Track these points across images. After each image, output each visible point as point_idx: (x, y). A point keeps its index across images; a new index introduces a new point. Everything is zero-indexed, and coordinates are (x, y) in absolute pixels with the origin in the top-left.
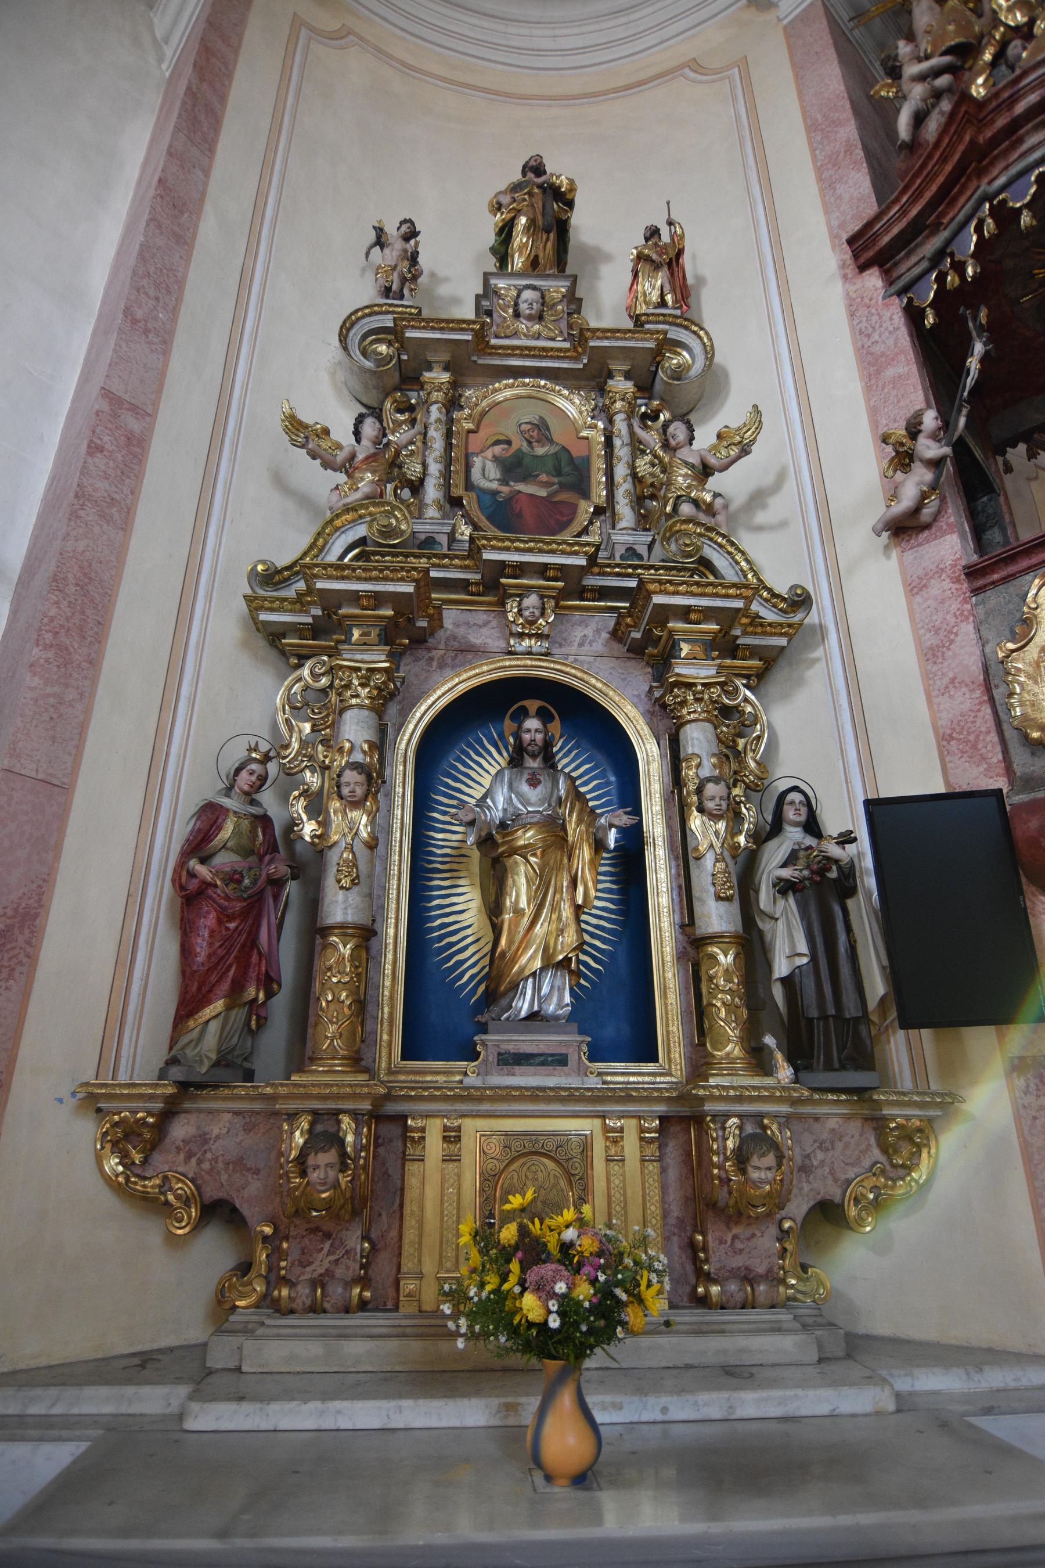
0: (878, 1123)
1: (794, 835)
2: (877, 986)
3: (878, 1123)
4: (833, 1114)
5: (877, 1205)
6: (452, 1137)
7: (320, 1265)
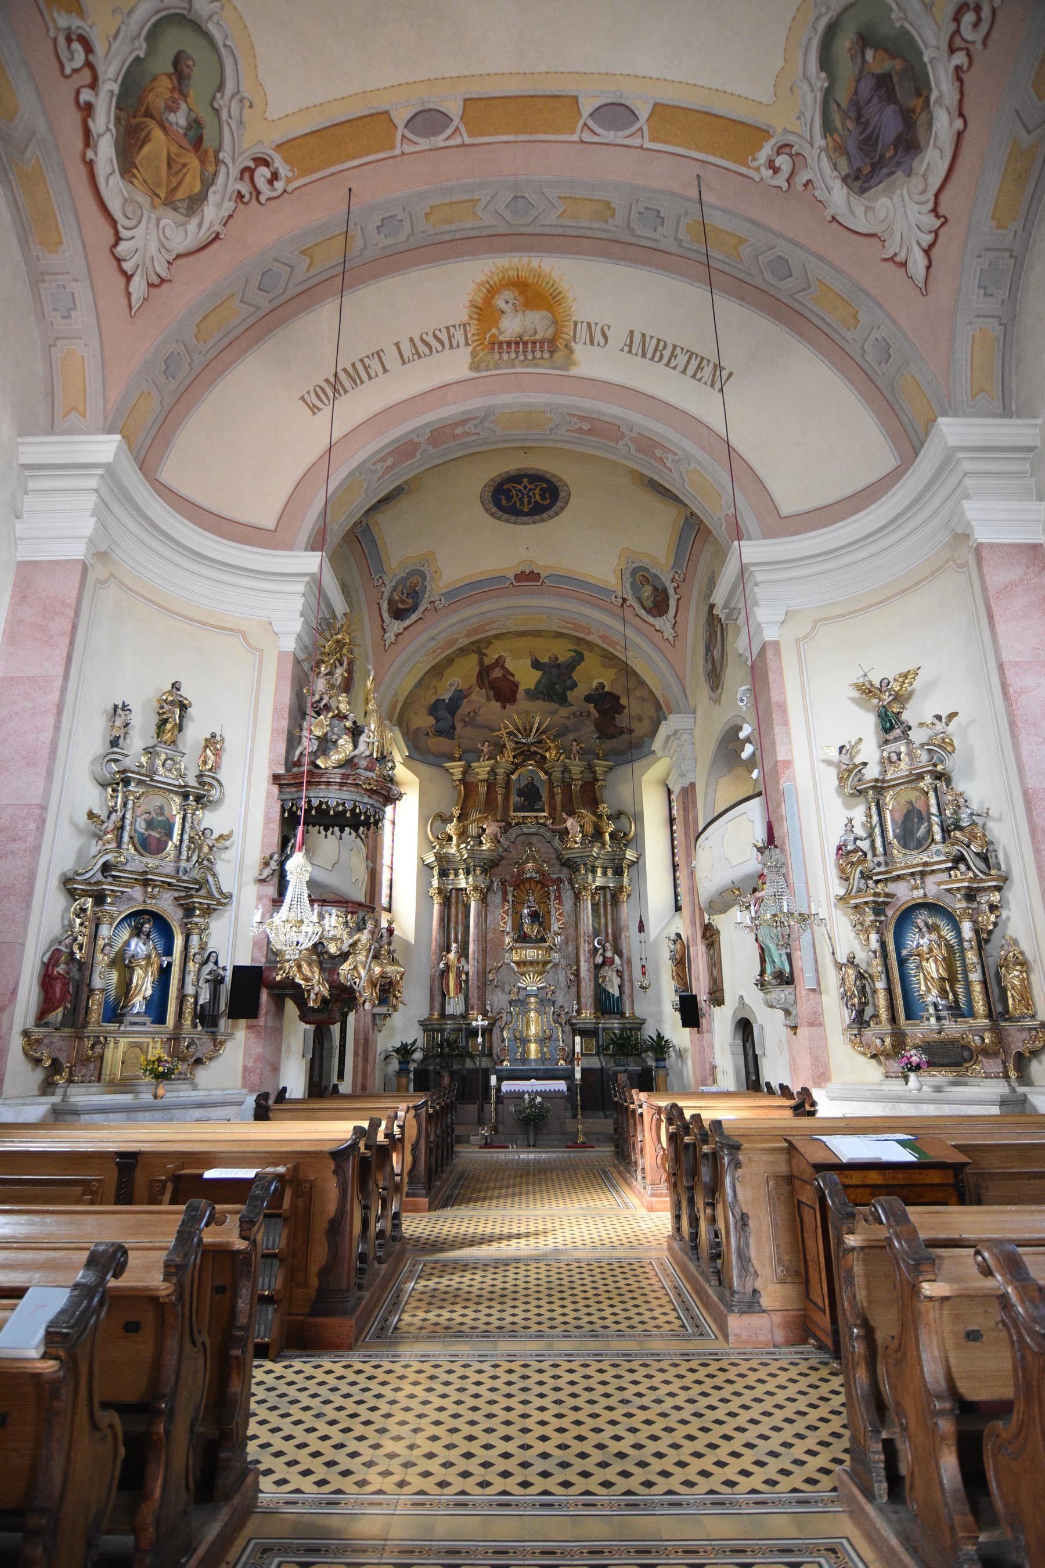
0: (215, 1040)
1: (210, 966)
2: (223, 1007)
3: (215, 1040)
4: (206, 1039)
5: (210, 1059)
6: (116, 1043)
7: (83, 1072)
